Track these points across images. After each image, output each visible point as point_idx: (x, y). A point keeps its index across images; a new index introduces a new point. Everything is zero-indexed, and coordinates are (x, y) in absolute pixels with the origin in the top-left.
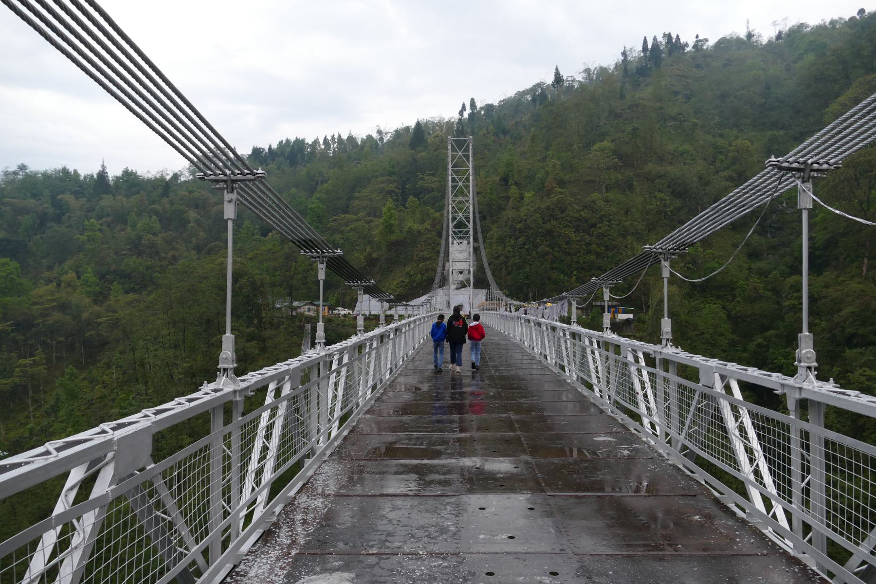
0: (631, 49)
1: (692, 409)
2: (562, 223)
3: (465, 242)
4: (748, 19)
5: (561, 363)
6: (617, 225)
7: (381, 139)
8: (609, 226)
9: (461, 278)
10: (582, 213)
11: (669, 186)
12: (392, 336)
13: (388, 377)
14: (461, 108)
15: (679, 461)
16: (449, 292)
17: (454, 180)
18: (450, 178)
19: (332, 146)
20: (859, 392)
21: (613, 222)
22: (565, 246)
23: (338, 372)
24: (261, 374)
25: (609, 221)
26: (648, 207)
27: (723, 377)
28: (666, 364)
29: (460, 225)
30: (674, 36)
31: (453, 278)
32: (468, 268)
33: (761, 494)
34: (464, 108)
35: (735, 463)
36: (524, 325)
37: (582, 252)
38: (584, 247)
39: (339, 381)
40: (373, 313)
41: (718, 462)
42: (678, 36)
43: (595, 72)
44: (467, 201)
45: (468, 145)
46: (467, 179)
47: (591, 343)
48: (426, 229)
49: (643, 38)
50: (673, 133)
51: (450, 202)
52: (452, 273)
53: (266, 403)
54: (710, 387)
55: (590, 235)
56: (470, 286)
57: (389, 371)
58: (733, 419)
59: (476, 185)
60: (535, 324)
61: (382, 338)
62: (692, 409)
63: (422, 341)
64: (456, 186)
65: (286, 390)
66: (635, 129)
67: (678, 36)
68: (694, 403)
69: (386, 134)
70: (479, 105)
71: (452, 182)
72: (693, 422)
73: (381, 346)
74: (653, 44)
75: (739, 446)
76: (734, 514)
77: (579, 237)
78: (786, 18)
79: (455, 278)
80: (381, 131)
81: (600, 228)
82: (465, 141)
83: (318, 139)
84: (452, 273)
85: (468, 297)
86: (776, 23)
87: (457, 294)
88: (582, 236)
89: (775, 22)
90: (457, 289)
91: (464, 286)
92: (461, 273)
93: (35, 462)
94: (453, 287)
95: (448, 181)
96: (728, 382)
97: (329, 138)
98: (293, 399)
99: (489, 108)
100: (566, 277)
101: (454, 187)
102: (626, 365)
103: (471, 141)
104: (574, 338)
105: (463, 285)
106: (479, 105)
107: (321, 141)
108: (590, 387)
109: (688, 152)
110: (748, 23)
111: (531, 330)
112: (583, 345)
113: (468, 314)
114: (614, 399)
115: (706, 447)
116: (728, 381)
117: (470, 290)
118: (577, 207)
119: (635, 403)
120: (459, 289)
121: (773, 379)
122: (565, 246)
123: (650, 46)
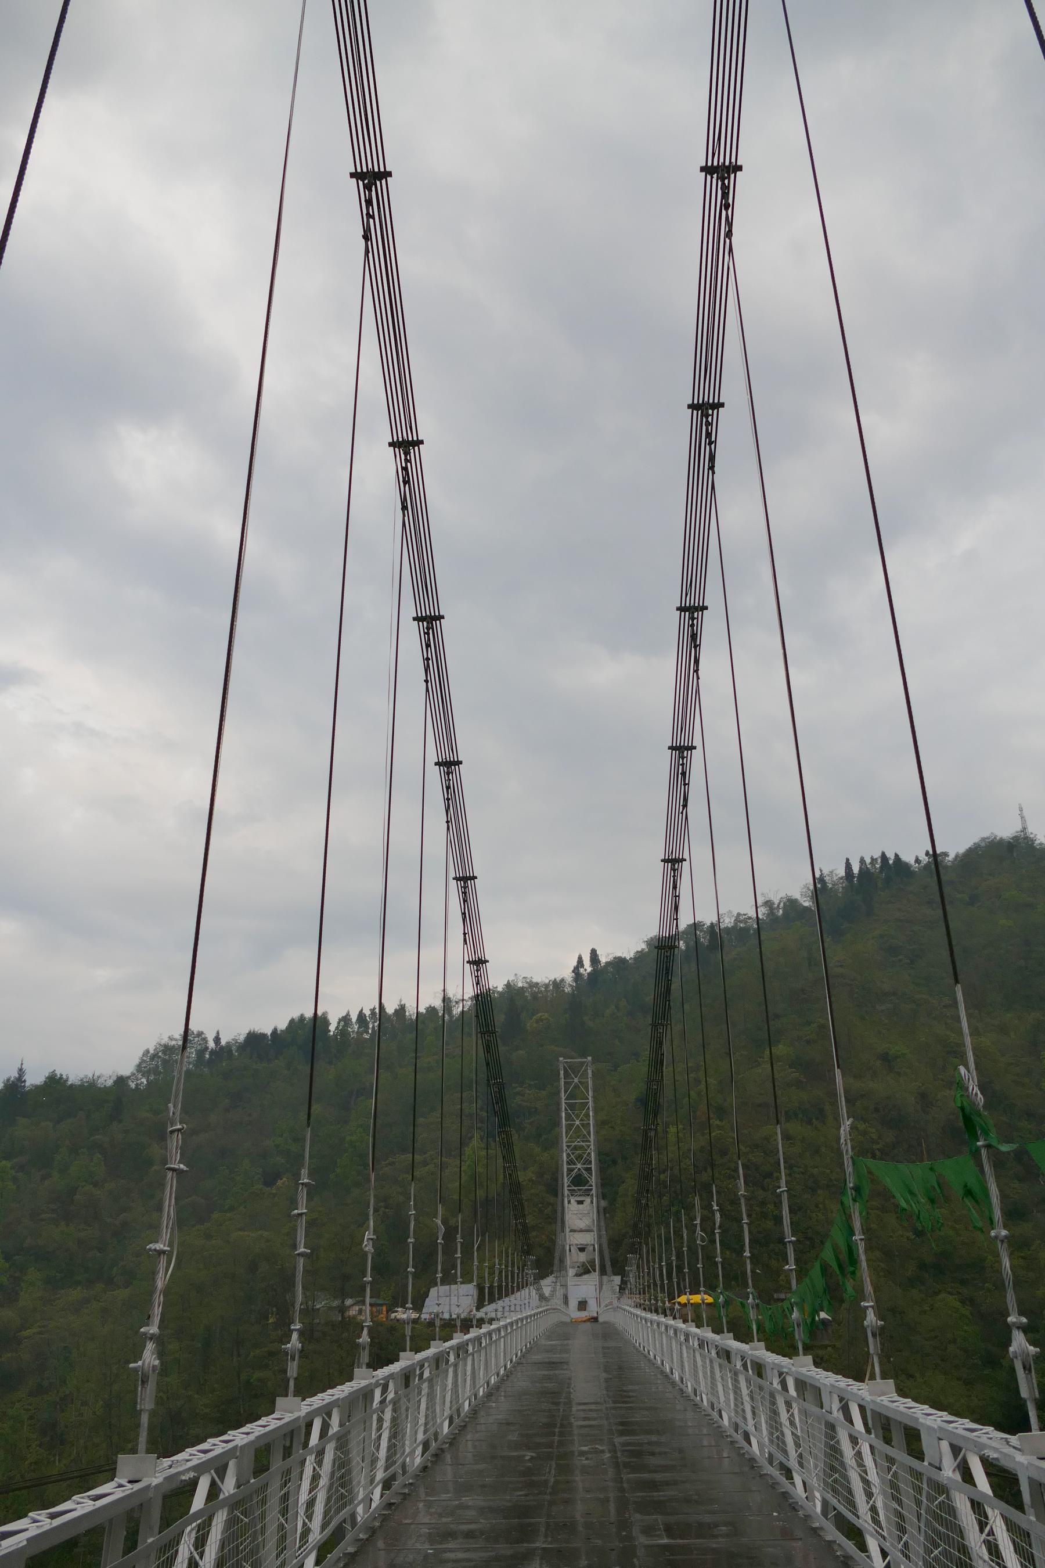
0: (831, 872)
2: (723, 1172)
3: (588, 1200)
6: (802, 1173)
9: (582, 1257)
11: (877, 1110)
12: (452, 1358)
13: (418, 1460)
14: (575, 963)
16: (566, 1281)
17: (568, 1117)
18: (563, 1115)
19: (371, 1026)
21: (796, 1169)
22: (729, 1208)
23: (320, 1453)
29: (579, 1181)
30: (891, 856)
31: (570, 1259)
32: (592, 1243)
34: (580, 961)
35: (998, 1558)
38: (758, 1209)
42: (896, 855)
43: (782, 905)
44: (589, 1146)
45: (586, 1070)
46: (587, 1116)
48: (531, 1180)
49: (845, 861)
51: (565, 1148)
52: (570, 1251)
55: (763, 1189)
57: (420, 1449)
61: (439, 1361)
63: (502, 1372)
64: (572, 1170)
65: (229, 1487)
67: (896, 855)
69: (457, 1003)
73: (438, 1376)
74: (860, 868)
83: (348, 1014)
84: (570, 1251)
85: (594, 1287)
87: (579, 1283)
90: (577, 1275)
92: (582, 1250)
93: (116, 1493)
94: (571, 1272)
95: (562, 1118)
97: (367, 1012)
99: (619, 963)
100: (734, 1255)
103: (589, 1064)
105: (585, 1270)
107: (354, 1018)
110: (1021, 810)
113: (595, 1315)
117: (594, 1277)
122: (729, 1208)
123: (856, 870)
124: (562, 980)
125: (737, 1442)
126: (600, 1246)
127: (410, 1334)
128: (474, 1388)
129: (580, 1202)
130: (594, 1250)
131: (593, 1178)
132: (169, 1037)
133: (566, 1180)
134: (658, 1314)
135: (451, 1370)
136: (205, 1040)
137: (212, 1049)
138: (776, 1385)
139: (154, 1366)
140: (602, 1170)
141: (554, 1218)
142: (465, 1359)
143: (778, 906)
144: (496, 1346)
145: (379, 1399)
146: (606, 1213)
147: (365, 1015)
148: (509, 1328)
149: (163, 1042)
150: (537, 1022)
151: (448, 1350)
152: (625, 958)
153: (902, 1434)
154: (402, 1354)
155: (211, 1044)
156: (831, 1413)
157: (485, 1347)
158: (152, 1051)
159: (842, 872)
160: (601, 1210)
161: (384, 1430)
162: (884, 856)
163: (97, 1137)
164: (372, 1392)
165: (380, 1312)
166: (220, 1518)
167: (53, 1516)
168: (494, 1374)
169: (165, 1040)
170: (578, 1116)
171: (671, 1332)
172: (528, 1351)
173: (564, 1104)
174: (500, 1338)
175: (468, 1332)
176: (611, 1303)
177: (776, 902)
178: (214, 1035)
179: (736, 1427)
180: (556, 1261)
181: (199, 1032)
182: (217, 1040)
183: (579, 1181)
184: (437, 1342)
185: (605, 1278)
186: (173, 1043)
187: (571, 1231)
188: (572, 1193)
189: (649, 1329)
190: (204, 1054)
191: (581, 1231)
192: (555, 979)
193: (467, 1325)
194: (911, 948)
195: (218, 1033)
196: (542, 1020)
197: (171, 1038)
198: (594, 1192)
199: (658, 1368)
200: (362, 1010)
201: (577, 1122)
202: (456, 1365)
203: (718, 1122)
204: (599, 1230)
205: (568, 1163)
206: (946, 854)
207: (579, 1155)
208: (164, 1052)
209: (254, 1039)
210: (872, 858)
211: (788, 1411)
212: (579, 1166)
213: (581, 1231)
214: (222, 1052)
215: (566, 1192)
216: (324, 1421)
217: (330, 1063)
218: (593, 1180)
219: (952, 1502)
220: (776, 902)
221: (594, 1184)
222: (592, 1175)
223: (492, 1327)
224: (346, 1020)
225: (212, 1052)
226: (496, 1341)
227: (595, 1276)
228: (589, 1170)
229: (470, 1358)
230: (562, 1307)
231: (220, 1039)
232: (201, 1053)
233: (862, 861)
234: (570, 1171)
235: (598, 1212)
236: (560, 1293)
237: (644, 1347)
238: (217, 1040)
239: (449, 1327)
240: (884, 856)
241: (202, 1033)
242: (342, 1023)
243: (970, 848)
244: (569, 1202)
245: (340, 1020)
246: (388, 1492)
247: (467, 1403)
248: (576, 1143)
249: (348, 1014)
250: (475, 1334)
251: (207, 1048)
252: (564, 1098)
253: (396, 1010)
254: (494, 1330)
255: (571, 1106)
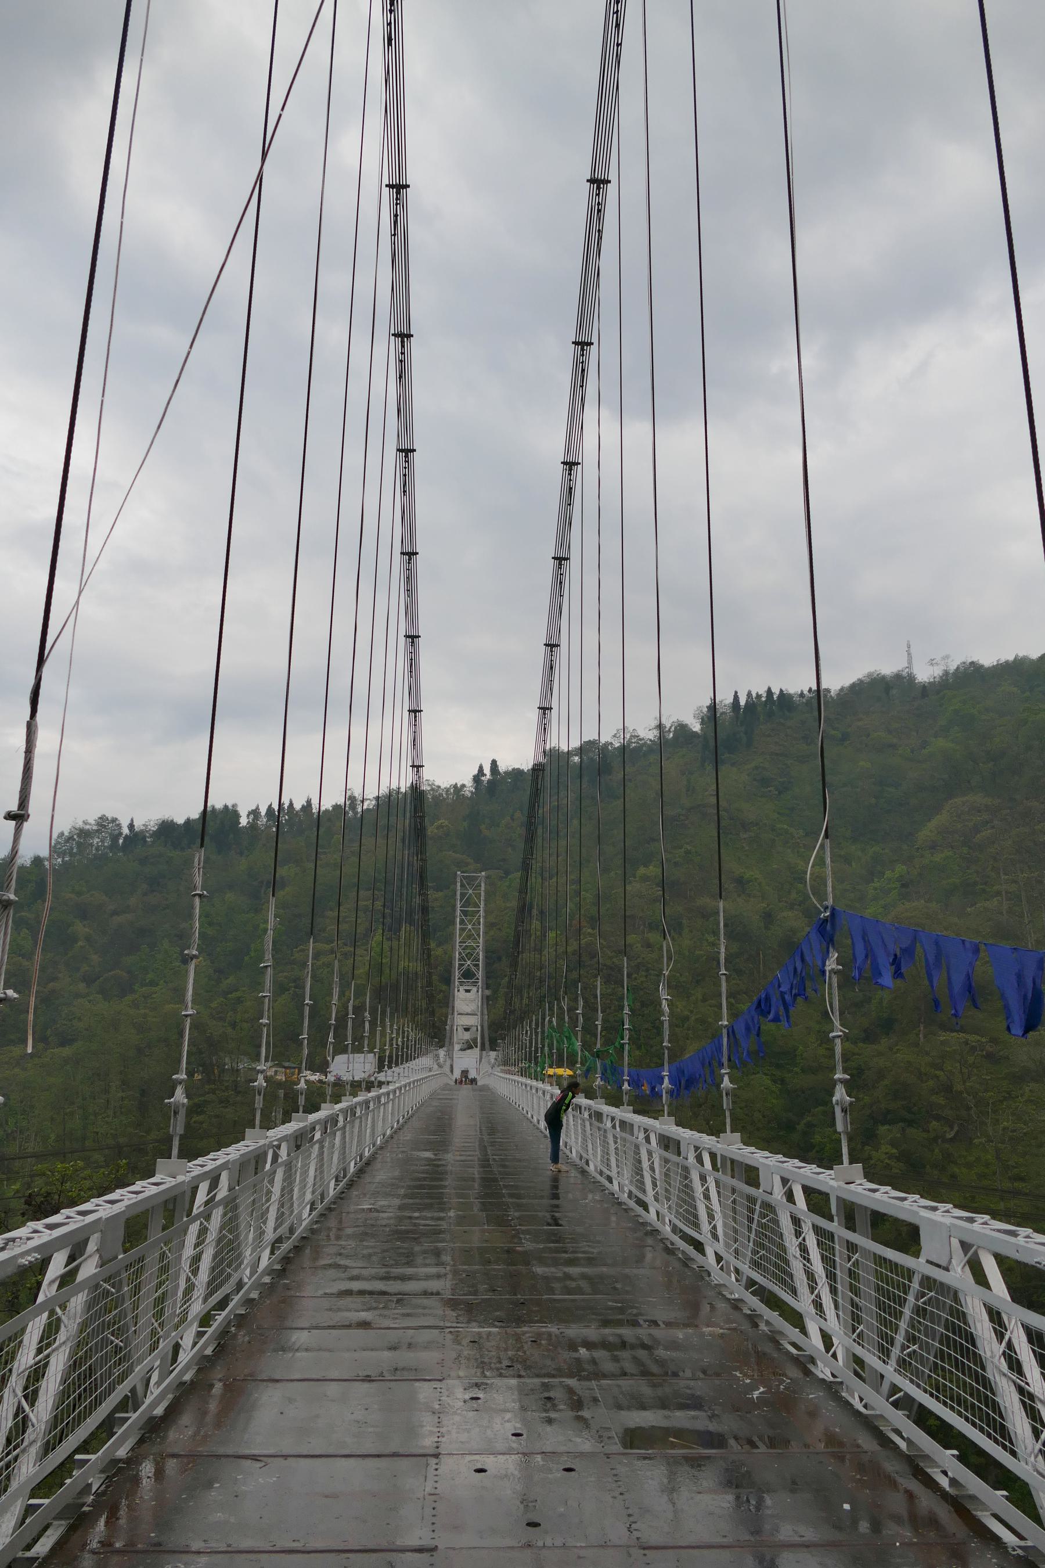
1: (907, 1312)
3: (475, 989)
4: (908, 641)
5: (608, 1173)
7: (353, 806)
8: (646, 976)
9: (467, 1036)
10: (614, 960)
15: (738, 1292)
17: (462, 922)
18: (458, 920)
20: (1031, 1230)
24: (51, 1227)
25: (647, 970)
26: (697, 952)
27: (785, 1181)
28: (851, 1214)
30: (776, 691)
31: (457, 1037)
32: (476, 1024)
33: (821, 1330)
34: (481, 768)
36: (587, 1124)
37: (613, 1008)
39: (46, 1365)
40: (356, 1079)
41: (762, 1280)
42: (781, 690)
43: (673, 728)
47: (699, 1159)
50: (747, 848)
53: (41, 1298)
54: (768, 1193)
56: (477, 1047)
58: (710, 1188)
59: (486, 942)
60: (590, 1116)
62: (907, 1312)
64: (463, 965)
66: (688, 852)
68: (911, 1298)
70: (502, 767)
71: (460, 924)
72: (911, 1339)
75: (797, 1267)
76: (997, 1539)
77: (610, 990)
78: (947, 657)
79: (460, 1036)
80: (355, 797)
81: (636, 979)
82: (476, 878)
83: (258, 808)
86: (934, 662)
88: (614, 989)
89: (932, 660)
91: (470, 1047)
92: (467, 1029)
96: (976, 1253)
98: (231, 1204)
101: (462, 930)
102: (686, 1169)
104: (666, 1148)
105: (469, 1046)
106: (502, 767)
107: (263, 811)
108: (645, 1206)
109: (756, 879)
110: (909, 647)
111: (605, 1137)
112: (685, 1163)
114: (748, 1277)
115: (937, 1391)
116: (791, 1186)
118: (609, 953)
119: (696, 1226)
120: (464, 1050)
121: (1021, 1240)
123: (743, 702)
124: (463, 786)
125: (632, 1209)
126: (482, 1027)
127: (261, 1106)
128: (373, 1137)
129: (468, 991)
130: (477, 1030)
131: (480, 973)
132: (84, 822)
133: (457, 974)
134: (537, 1080)
135: (338, 1134)
136: (119, 826)
137: (126, 835)
138: (692, 1159)
139: (183, 1104)
140: (488, 964)
141: (448, 1002)
142: (352, 1122)
143: (669, 729)
144: (384, 1108)
145: (62, 1271)
146: (488, 1001)
147: (274, 809)
148: (398, 1092)
149: (77, 826)
150: (437, 828)
151: (275, 1143)
152: (523, 770)
153: (867, 1223)
154: (323, 1105)
155: (126, 831)
156: (771, 1194)
157: (373, 1110)
158: (66, 834)
159: (731, 700)
160: (485, 997)
161: (60, 1346)
162: (769, 692)
163: (23, 914)
164: (265, 1154)
165: (293, 1074)
166: (217, 1216)
167: (51, 1227)
168: (380, 1135)
169: (80, 824)
170: (470, 921)
171: (540, 1093)
172: (423, 1105)
173: (459, 911)
174: (388, 1102)
175: (340, 1102)
176: (487, 1072)
177: (668, 726)
178: (129, 822)
179: (601, 1173)
180: (447, 1040)
181: (113, 818)
182: (131, 826)
183: (468, 975)
184: (376, 1089)
185: (484, 1052)
186: (88, 827)
187: (459, 1014)
188: (461, 984)
189: (529, 1093)
190: (119, 839)
191: (467, 1014)
192: (456, 784)
193: (369, 1086)
194: (781, 780)
195: (132, 820)
196: (442, 827)
197: (85, 823)
198: (480, 984)
199: (534, 1125)
200: (271, 805)
201: (470, 927)
202: (321, 1142)
203: (589, 930)
204: (482, 1014)
205: (460, 960)
206: (828, 691)
207: (469, 954)
208: (79, 836)
209: (167, 828)
210: (757, 693)
211: (703, 1185)
212: (469, 962)
213: (467, 1014)
214: (136, 837)
215: (457, 983)
216: (274, 1152)
217: (241, 854)
218: (480, 974)
219: (970, 1328)
220: (668, 726)
221: (480, 978)
222: (478, 969)
223: (381, 1091)
224: (255, 813)
225: (126, 837)
226: (384, 1104)
227: (476, 1051)
228: (477, 966)
229: (357, 1121)
230: (449, 1073)
231: (134, 826)
232: (115, 838)
233: (749, 694)
234: (461, 965)
235: (482, 999)
236: (448, 1063)
237: (523, 1109)
238: (131, 826)
239: (339, 1090)
240: (769, 692)
241: (116, 819)
242: (252, 817)
243: (853, 683)
244: (458, 991)
245: (249, 814)
246: (46, 1501)
247: (352, 1164)
248: (466, 944)
249: (258, 808)
250: (365, 1098)
251: (121, 834)
252: (459, 906)
253: (303, 806)
254: (383, 1094)
255: (465, 913)
